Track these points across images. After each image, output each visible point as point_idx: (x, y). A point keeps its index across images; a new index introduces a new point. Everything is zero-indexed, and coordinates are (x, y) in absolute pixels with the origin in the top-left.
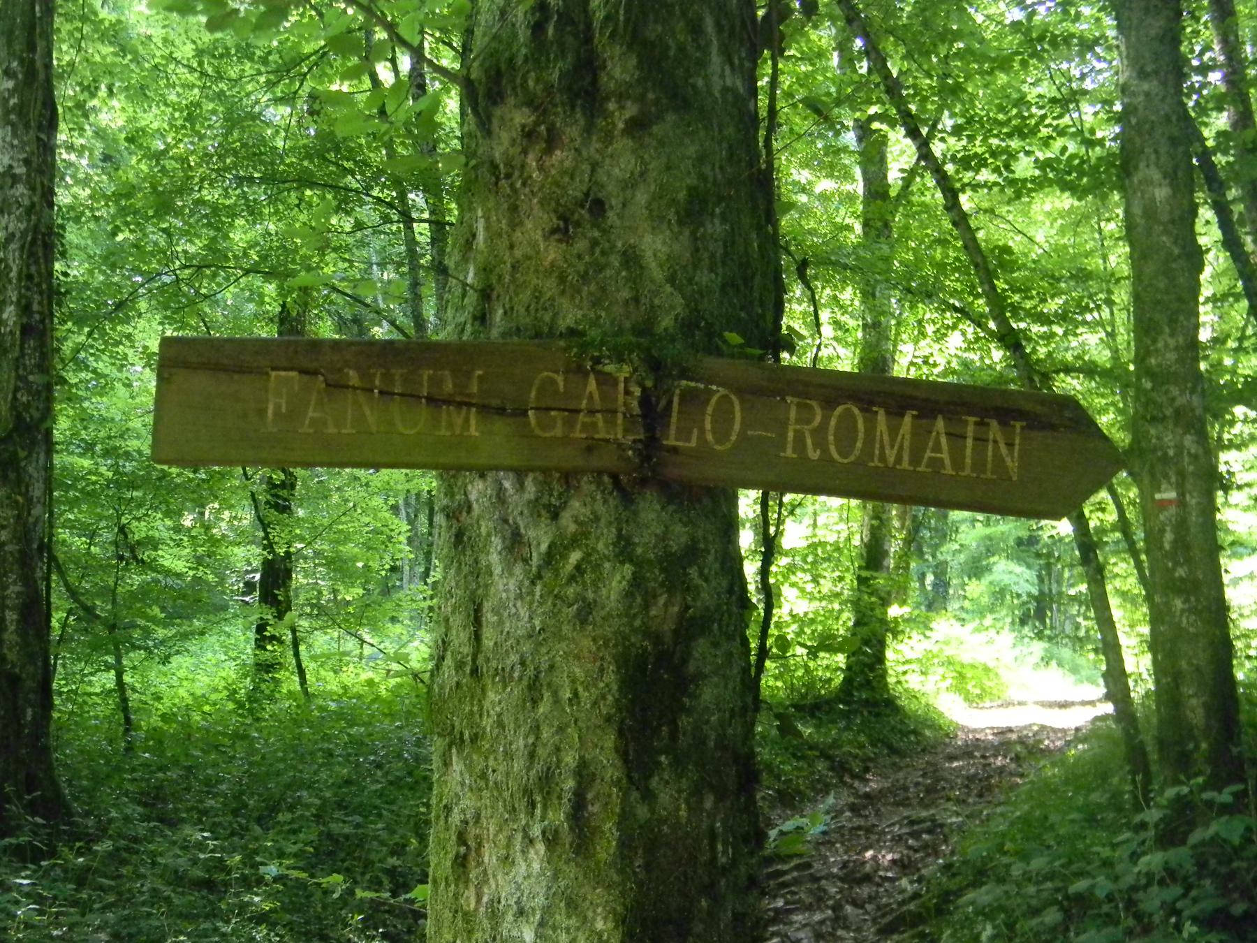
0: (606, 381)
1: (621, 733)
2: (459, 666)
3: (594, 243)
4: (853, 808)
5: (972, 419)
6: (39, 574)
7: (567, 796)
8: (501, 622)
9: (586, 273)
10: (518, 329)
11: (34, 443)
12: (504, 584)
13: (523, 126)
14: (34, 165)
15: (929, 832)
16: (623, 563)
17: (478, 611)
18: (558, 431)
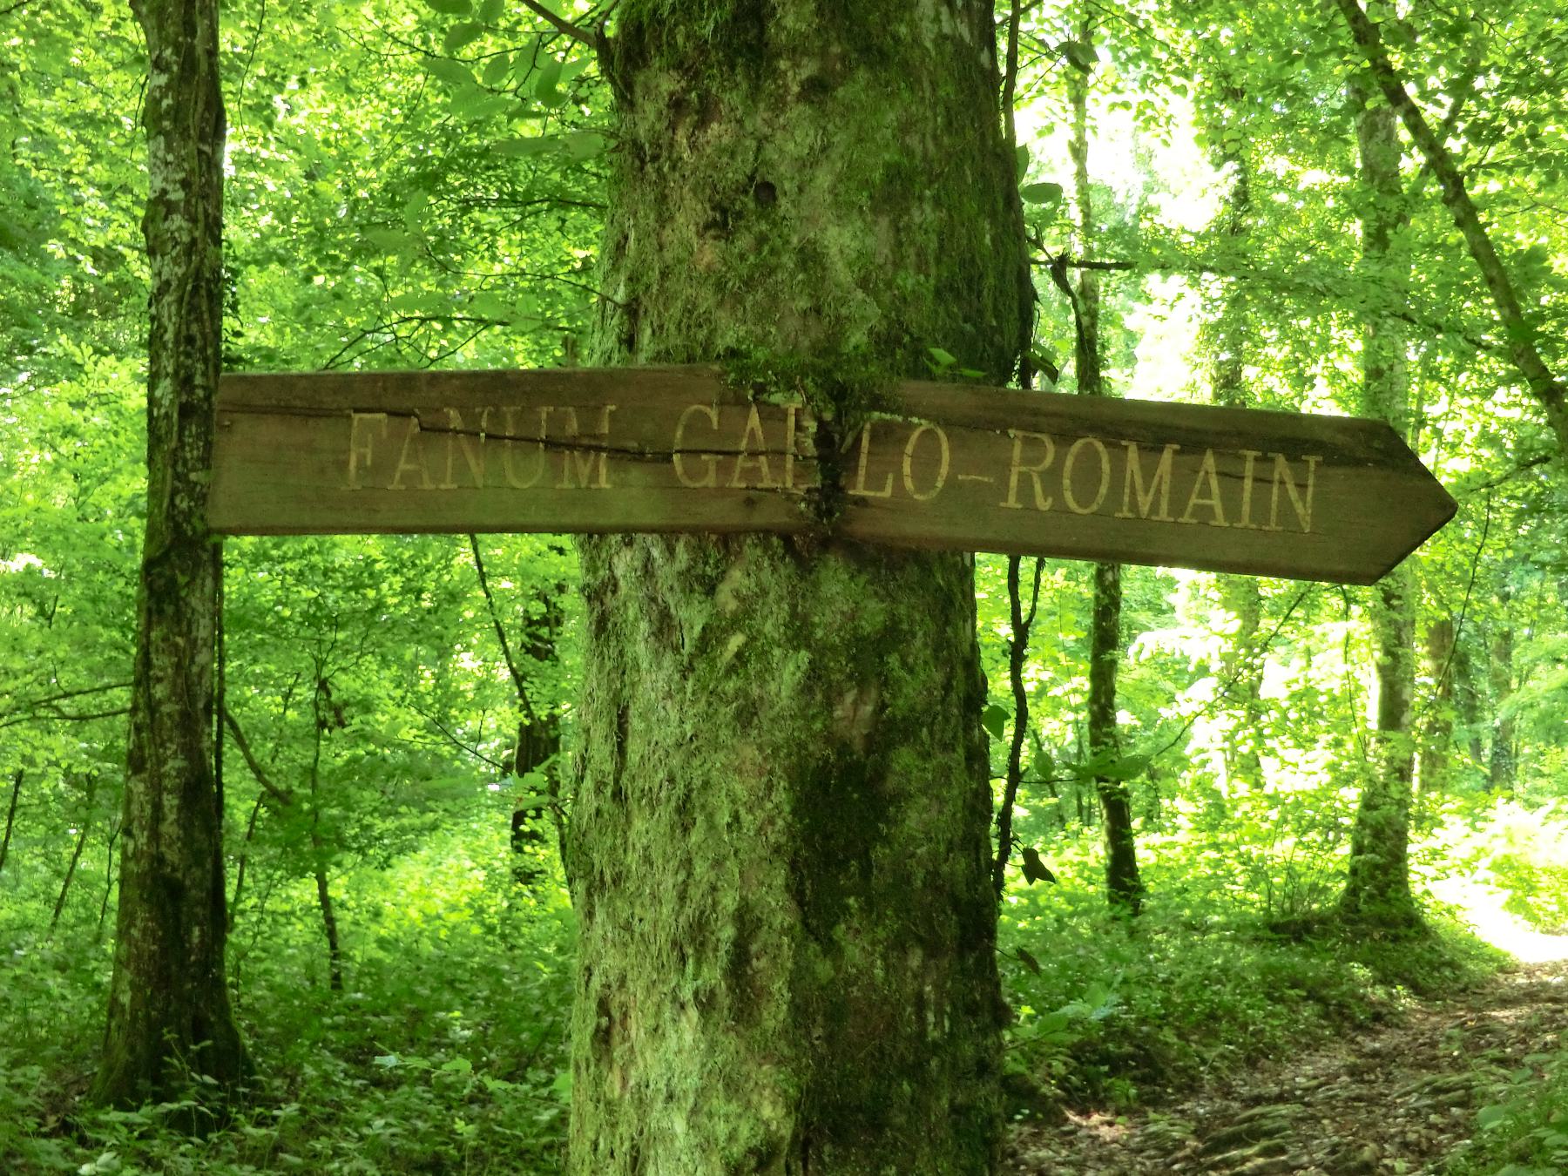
0: (772, 415)
1: (793, 866)
2: (599, 787)
3: (762, 239)
4: (1353, 1071)
5: (1251, 454)
6: (206, 744)
7: (724, 947)
8: (649, 730)
9: (751, 278)
10: (668, 352)
11: (198, 564)
12: (653, 678)
13: (671, 94)
14: (195, 188)
15: (1461, 1104)
16: (796, 649)
17: (622, 717)
18: (710, 481)
